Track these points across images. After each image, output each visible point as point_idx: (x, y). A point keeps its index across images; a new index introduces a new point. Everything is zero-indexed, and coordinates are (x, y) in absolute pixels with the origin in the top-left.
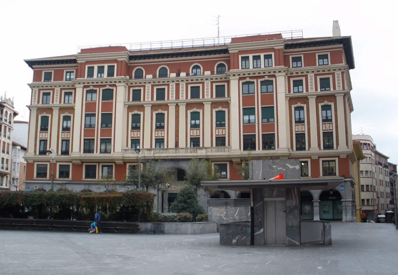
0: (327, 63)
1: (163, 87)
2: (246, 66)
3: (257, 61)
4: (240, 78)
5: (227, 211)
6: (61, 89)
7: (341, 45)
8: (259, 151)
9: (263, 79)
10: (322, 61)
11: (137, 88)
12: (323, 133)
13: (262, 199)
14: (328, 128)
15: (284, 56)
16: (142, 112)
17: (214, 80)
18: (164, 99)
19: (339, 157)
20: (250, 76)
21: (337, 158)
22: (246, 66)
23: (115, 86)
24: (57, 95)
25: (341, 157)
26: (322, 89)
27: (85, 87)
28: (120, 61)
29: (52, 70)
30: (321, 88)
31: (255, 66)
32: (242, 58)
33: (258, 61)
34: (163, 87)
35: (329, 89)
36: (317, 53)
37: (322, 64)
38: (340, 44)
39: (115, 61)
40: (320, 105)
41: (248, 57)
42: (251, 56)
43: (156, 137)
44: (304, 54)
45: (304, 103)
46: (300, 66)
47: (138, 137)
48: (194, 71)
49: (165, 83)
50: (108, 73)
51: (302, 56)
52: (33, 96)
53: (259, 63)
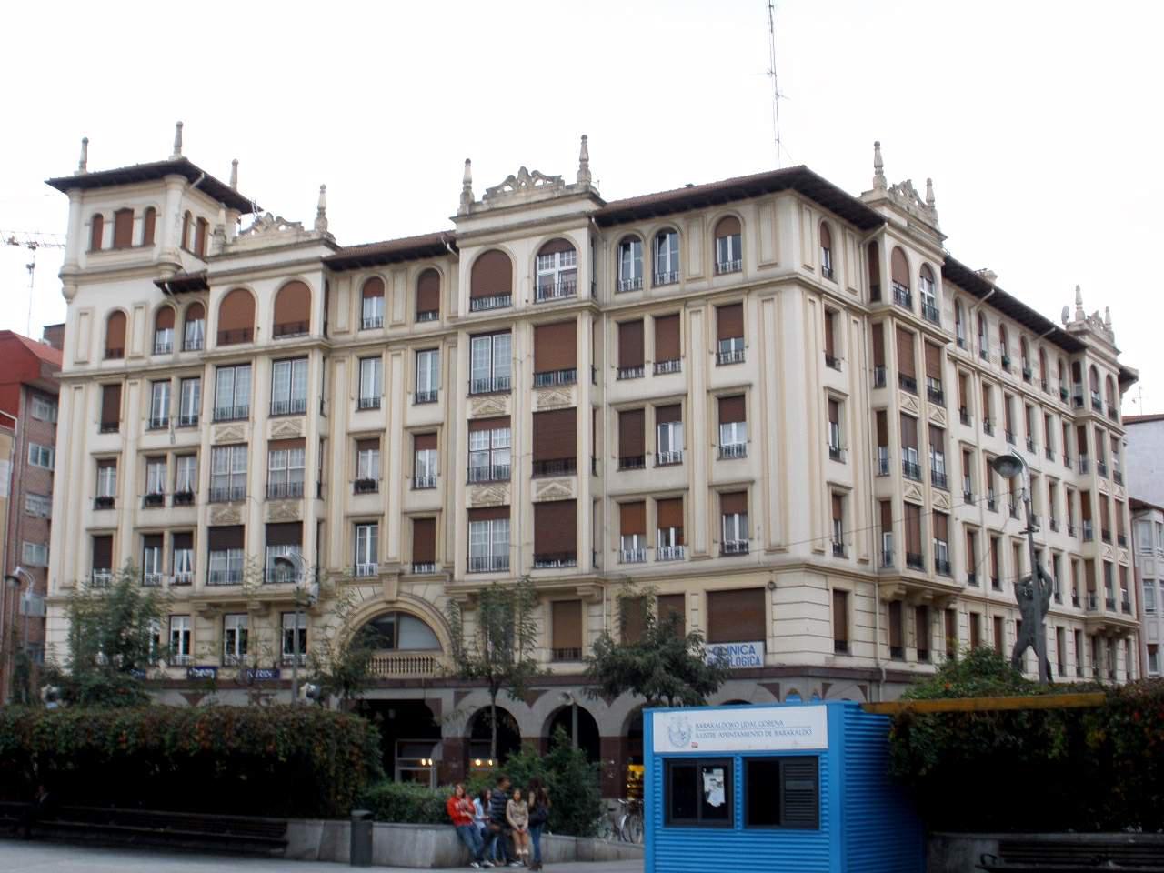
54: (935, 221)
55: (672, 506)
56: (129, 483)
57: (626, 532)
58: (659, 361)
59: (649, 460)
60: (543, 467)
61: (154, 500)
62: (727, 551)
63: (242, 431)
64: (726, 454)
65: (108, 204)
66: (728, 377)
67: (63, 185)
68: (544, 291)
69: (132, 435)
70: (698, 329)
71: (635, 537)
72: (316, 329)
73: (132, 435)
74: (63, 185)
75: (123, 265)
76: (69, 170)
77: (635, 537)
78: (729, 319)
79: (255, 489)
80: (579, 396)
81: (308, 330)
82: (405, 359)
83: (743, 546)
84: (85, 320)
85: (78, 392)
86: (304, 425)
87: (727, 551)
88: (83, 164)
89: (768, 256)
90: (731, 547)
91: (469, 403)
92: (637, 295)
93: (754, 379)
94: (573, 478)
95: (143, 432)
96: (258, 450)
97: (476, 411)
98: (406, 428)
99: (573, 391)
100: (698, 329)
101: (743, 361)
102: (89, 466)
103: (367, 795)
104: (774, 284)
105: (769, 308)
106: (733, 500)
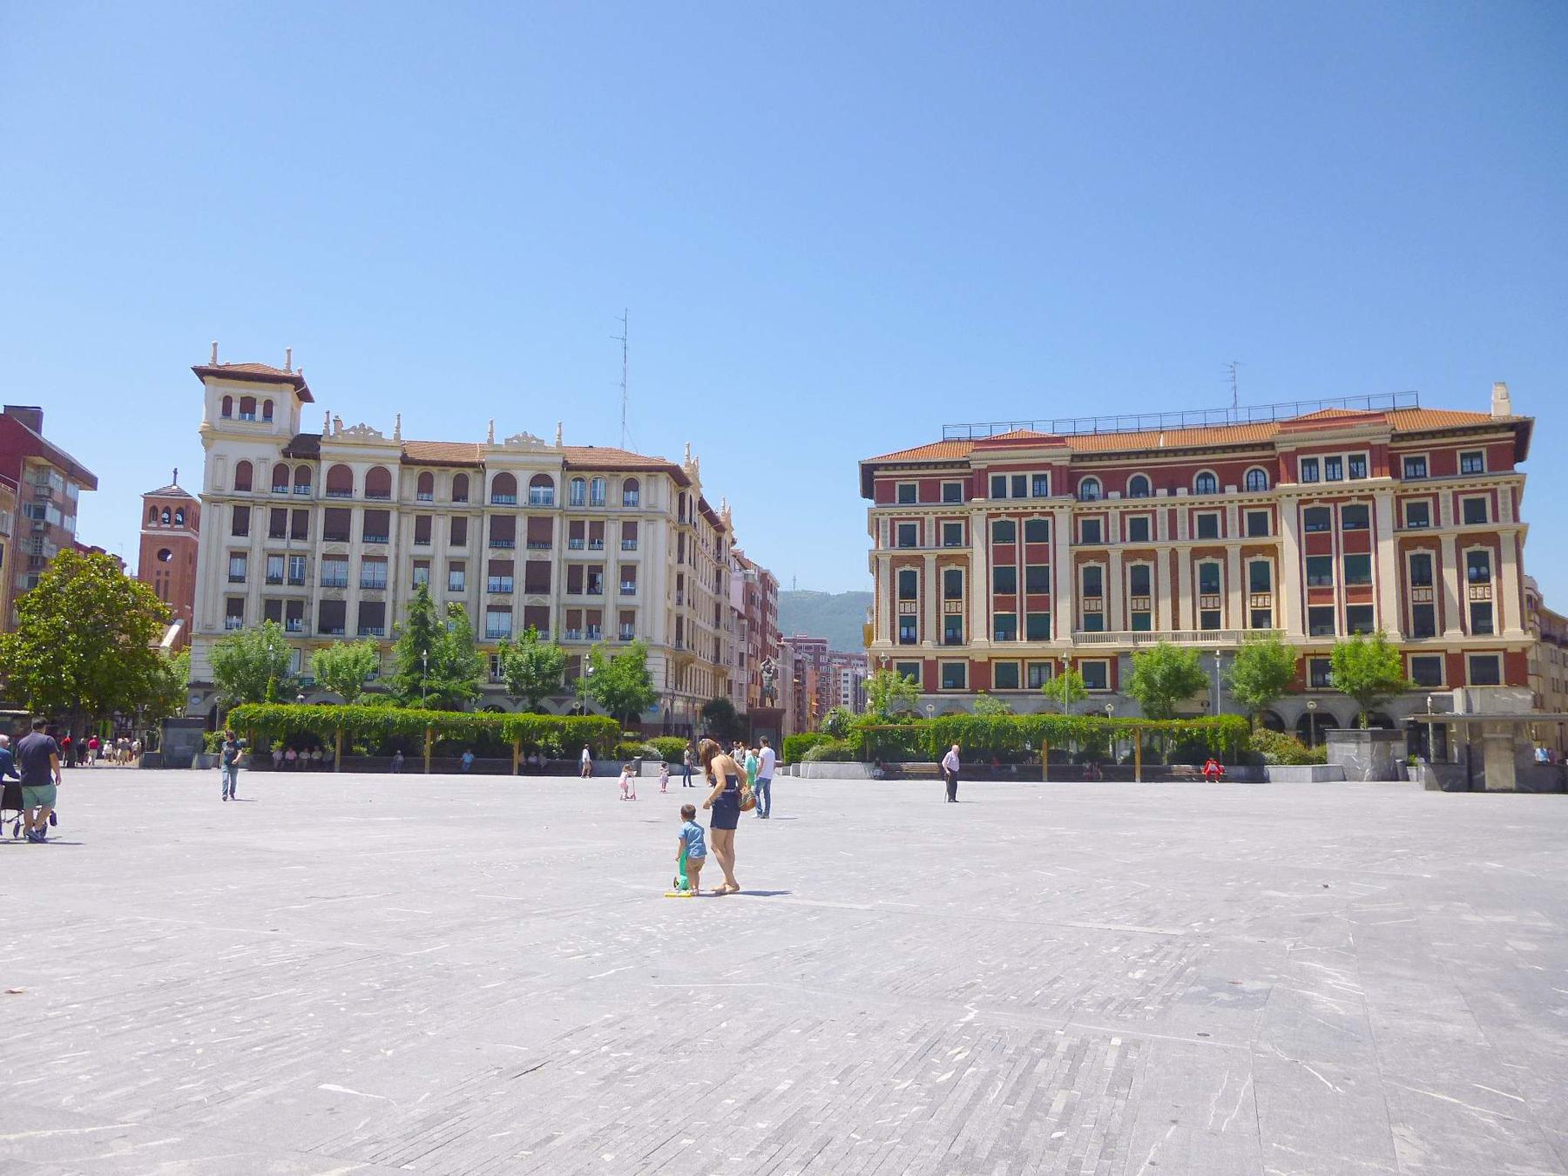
0: (1479, 469)
1: (1145, 516)
2: (1334, 474)
3: (1334, 467)
4: (1300, 500)
5: (1359, 749)
6: (936, 518)
7: (1512, 434)
8: (1341, 637)
9: (1347, 504)
10: (1412, 468)
11: (1091, 518)
12: (1472, 605)
13: (1480, 735)
14: (1093, 603)
15: (1390, 455)
16: (1273, 558)
17: (1196, 506)
18: (1265, 533)
19: (1445, 651)
20: (1320, 497)
21: (1502, 653)
22: (1334, 474)
23: (1371, 497)
24: (930, 531)
25: (1450, 651)
26: (1411, 524)
27: (1301, 502)
28: (1376, 446)
29: (1425, 451)
30: (1408, 522)
31: (1037, 493)
32: (1303, 461)
33: (1336, 467)
34: (1145, 516)
35: (1425, 523)
36: (1402, 453)
37: (1470, 470)
38: (1508, 431)
39: (1048, 466)
40: (1465, 551)
41: (1340, 458)
42: (1321, 458)
43: (1134, 610)
44: (1431, 452)
45: (1432, 547)
46: (1423, 473)
47: (1145, 609)
48: (1202, 482)
49: (1203, 506)
50: (552, 527)
51: (1427, 456)
52: (880, 531)
53: (1043, 488)
54: (1536, 587)
55: (595, 616)
56: (256, 568)
57: (569, 627)
58: (592, 542)
59: (585, 590)
60: (530, 589)
61: (274, 580)
62: (622, 638)
63: (345, 548)
64: (624, 592)
65: (238, 390)
66: (628, 556)
67: (201, 373)
68: (533, 499)
69: (258, 539)
70: (613, 532)
71: (627, 625)
72: (394, 496)
73: (258, 539)
74: (201, 373)
75: (1396, 569)
76: (205, 363)
77: (627, 625)
78: (630, 531)
79: (354, 582)
80: (552, 556)
81: (389, 495)
82: (266, 511)
83: (630, 636)
84: (220, 463)
85: (216, 508)
86: (348, 548)
87: (622, 638)
88: (214, 358)
89: (652, 501)
90: (624, 636)
91: (490, 551)
92: (582, 508)
93: (641, 559)
94: (548, 596)
95: (267, 538)
96: (355, 560)
97: (494, 555)
98: (446, 558)
99: (550, 552)
100: (613, 532)
101: (636, 550)
102: (225, 556)
103: (1258, 659)
104: (652, 516)
105: (651, 528)
106: (627, 617)
